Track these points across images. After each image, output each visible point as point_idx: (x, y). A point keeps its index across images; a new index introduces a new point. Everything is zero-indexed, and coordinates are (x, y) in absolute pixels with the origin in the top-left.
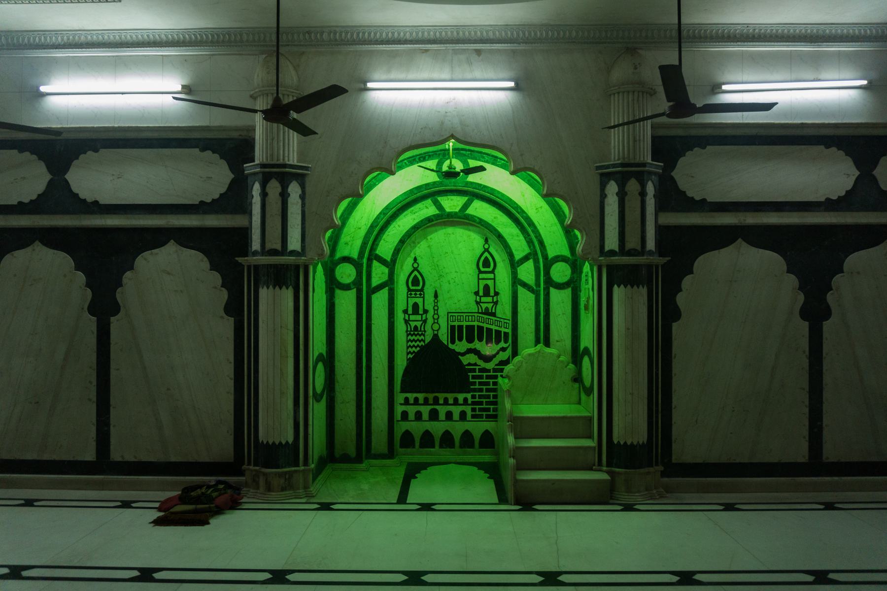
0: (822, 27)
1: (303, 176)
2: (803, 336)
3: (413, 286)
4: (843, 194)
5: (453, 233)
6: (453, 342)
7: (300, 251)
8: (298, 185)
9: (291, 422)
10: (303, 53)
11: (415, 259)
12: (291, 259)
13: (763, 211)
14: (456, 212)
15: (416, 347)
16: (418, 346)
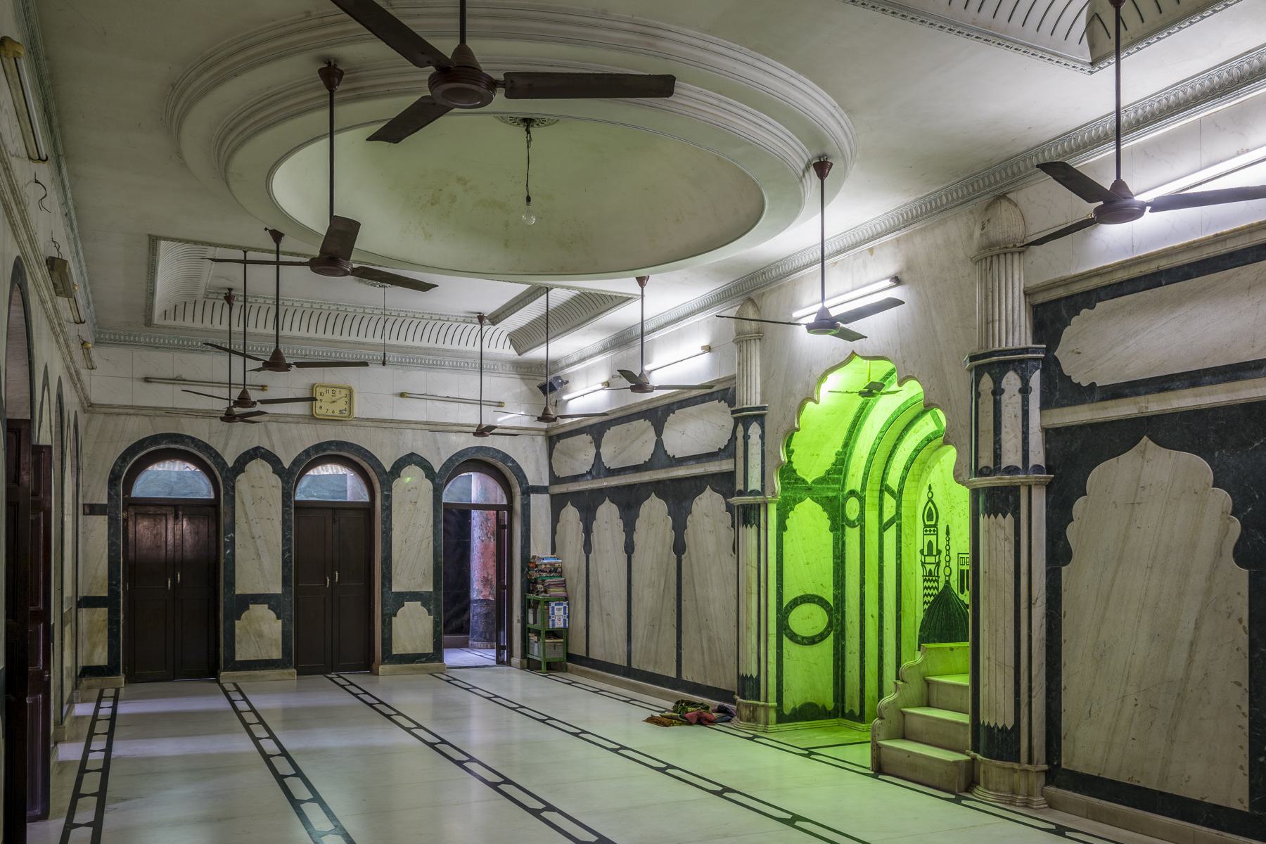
0: (1235, 63)
1: (762, 416)
3: (928, 520)
7: (760, 490)
8: (757, 425)
9: (755, 656)
10: (763, 294)
11: (930, 488)
12: (1006, 480)
13: (1173, 389)
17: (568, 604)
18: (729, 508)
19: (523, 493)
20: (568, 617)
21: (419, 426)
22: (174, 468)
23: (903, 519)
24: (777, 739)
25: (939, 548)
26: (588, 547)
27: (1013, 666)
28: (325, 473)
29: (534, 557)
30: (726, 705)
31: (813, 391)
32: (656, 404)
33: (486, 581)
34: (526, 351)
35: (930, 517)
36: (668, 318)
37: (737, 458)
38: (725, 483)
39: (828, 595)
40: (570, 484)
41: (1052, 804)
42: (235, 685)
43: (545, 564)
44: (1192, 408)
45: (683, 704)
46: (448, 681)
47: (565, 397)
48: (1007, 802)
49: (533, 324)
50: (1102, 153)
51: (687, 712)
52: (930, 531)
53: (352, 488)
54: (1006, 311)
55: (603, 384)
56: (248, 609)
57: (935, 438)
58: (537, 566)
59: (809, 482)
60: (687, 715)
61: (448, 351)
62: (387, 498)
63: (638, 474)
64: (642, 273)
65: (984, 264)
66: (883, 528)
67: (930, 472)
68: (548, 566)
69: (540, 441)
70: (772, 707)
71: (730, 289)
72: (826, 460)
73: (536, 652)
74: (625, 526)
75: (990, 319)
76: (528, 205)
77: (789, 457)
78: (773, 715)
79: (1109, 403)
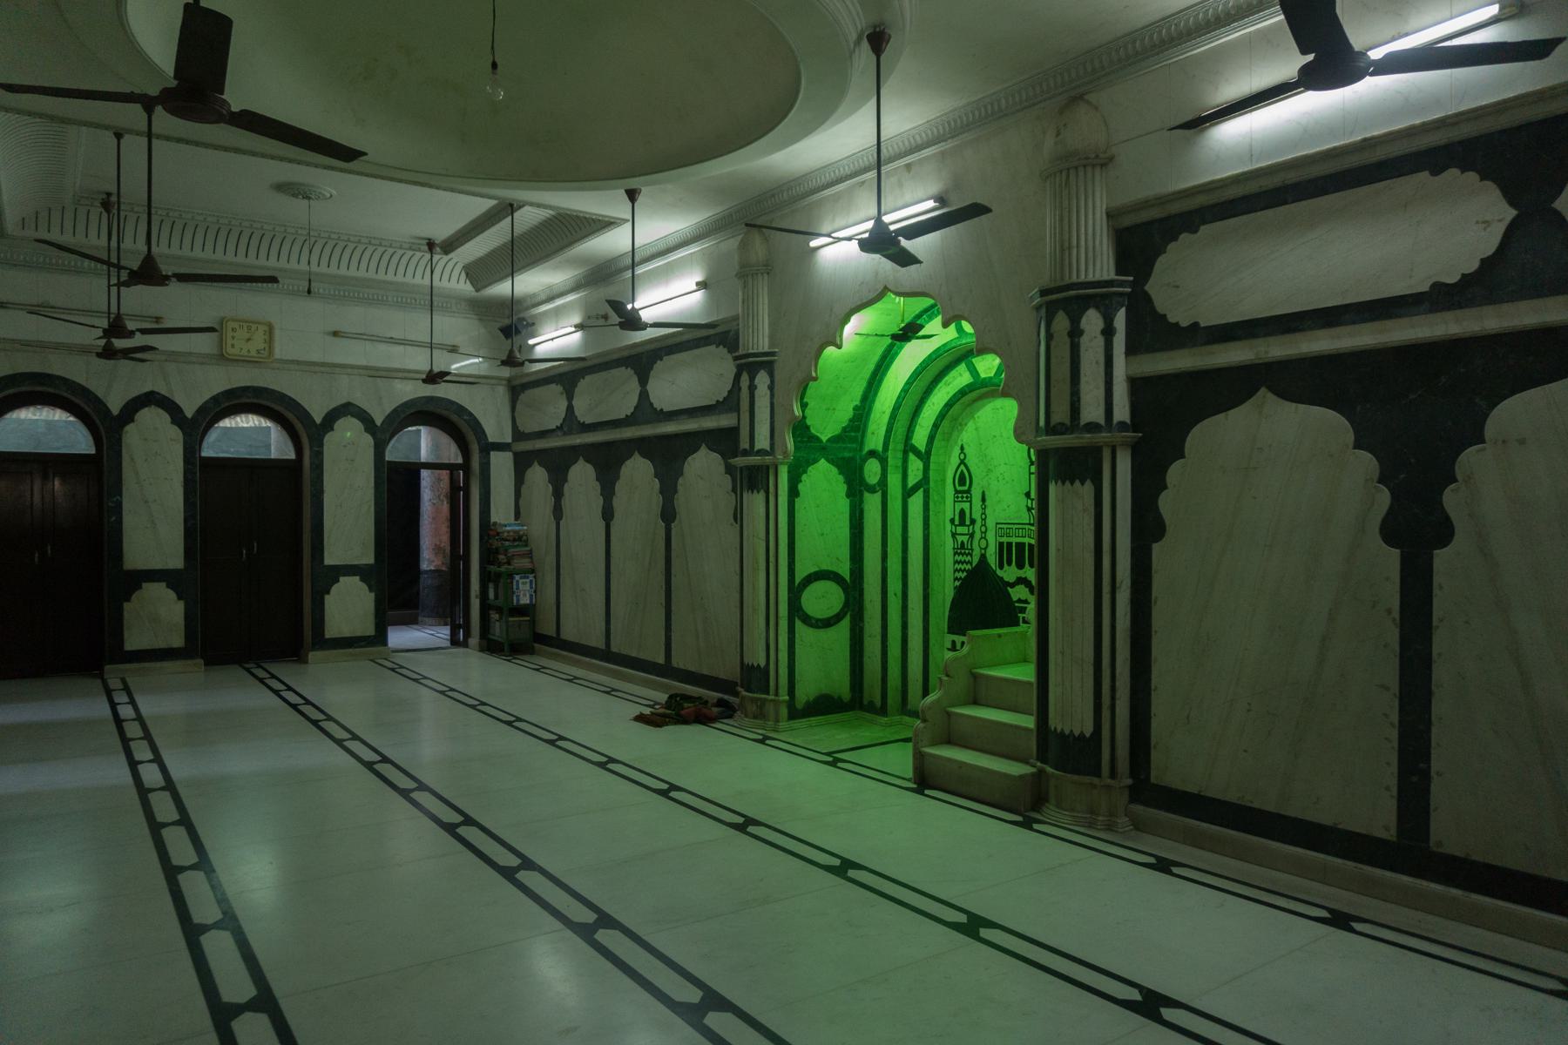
1: (771, 363)
2: (1387, 579)
4: (1474, 266)
5: (1002, 408)
6: (1001, 567)
7: (769, 449)
11: (962, 448)
12: (1086, 439)
14: (991, 378)
15: (963, 571)
16: (965, 569)
17: (535, 577)
18: (729, 470)
19: (481, 451)
20: (535, 592)
21: (356, 371)
22: (54, 415)
23: (932, 484)
24: (790, 740)
26: (558, 512)
27: (1092, 662)
28: (245, 425)
29: (495, 524)
30: (726, 697)
31: (835, 333)
32: (639, 350)
33: (438, 549)
34: (486, 287)
35: (962, 481)
36: (654, 250)
37: (741, 412)
38: (726, 442)
39: (845, 570)
40: (538, 441)
41: (1139, 826)
42: (124, 681)
43: (508, 532)
44: (1326, 353)
45: (678, 699)
46: (393, 670)
47: (531, 342)
48: (1087, 825)
49: (492, 255)
50: (1245, 28)
51: (683, 709)
52: (962, 497)
53: (275, 444)
54: (1086, 234)
55: (575, 327)
56: (141, 588)
57: (970, 392)
58: (498, 534)
59: (824, 441)
60: (683, 712)
61: (391, 283)
62: (318, 455)
63: (618, 430)
64: (633, 183)
65: (1058, 179)
66: (908, 493)
67: (962, 430)
68: (511, 534)
69: (502, 392)
70: (784, 701)
71: (731, 215)
72: (844, 413)
73: (497, 630)
74: (603, 489)
75: (1066, 244)
76: (493, 73)
77: (803, 412)
78: (784, 711)
79: (1216, 347)
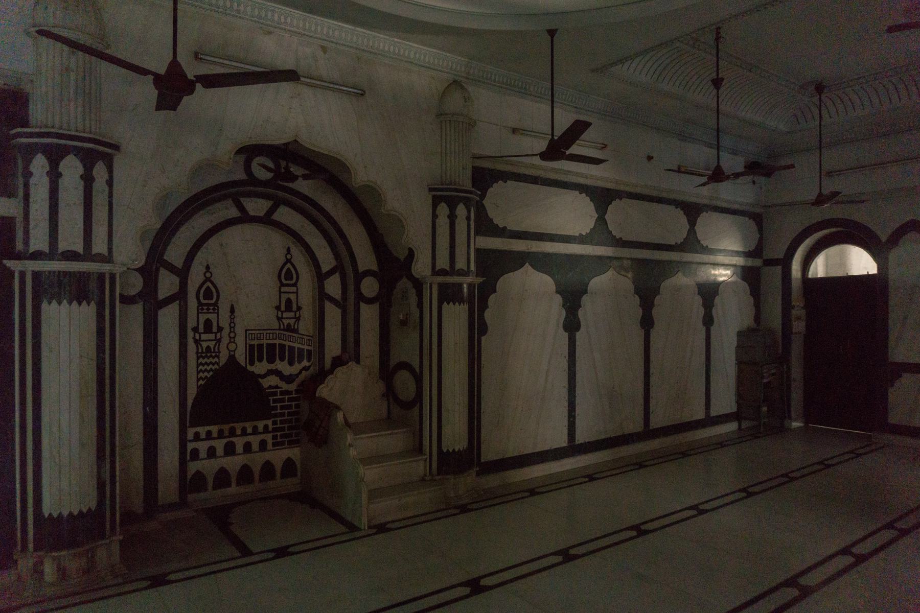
6: (252, 363)
11: (208, 267)
25: (299, 305)
35: (208, 294)
52: (208, 309)
